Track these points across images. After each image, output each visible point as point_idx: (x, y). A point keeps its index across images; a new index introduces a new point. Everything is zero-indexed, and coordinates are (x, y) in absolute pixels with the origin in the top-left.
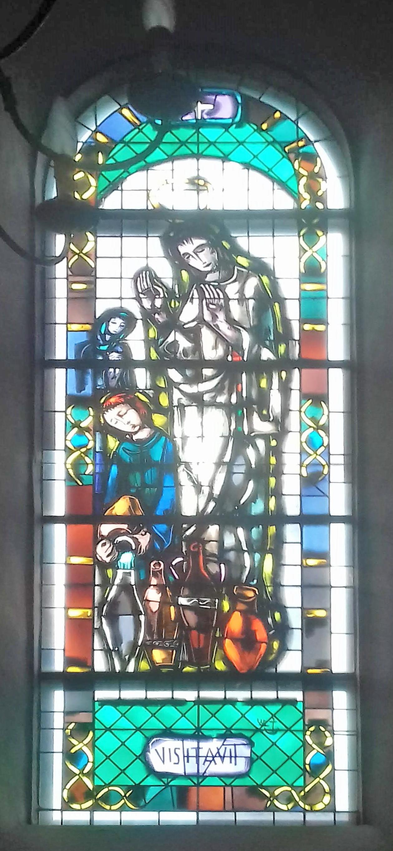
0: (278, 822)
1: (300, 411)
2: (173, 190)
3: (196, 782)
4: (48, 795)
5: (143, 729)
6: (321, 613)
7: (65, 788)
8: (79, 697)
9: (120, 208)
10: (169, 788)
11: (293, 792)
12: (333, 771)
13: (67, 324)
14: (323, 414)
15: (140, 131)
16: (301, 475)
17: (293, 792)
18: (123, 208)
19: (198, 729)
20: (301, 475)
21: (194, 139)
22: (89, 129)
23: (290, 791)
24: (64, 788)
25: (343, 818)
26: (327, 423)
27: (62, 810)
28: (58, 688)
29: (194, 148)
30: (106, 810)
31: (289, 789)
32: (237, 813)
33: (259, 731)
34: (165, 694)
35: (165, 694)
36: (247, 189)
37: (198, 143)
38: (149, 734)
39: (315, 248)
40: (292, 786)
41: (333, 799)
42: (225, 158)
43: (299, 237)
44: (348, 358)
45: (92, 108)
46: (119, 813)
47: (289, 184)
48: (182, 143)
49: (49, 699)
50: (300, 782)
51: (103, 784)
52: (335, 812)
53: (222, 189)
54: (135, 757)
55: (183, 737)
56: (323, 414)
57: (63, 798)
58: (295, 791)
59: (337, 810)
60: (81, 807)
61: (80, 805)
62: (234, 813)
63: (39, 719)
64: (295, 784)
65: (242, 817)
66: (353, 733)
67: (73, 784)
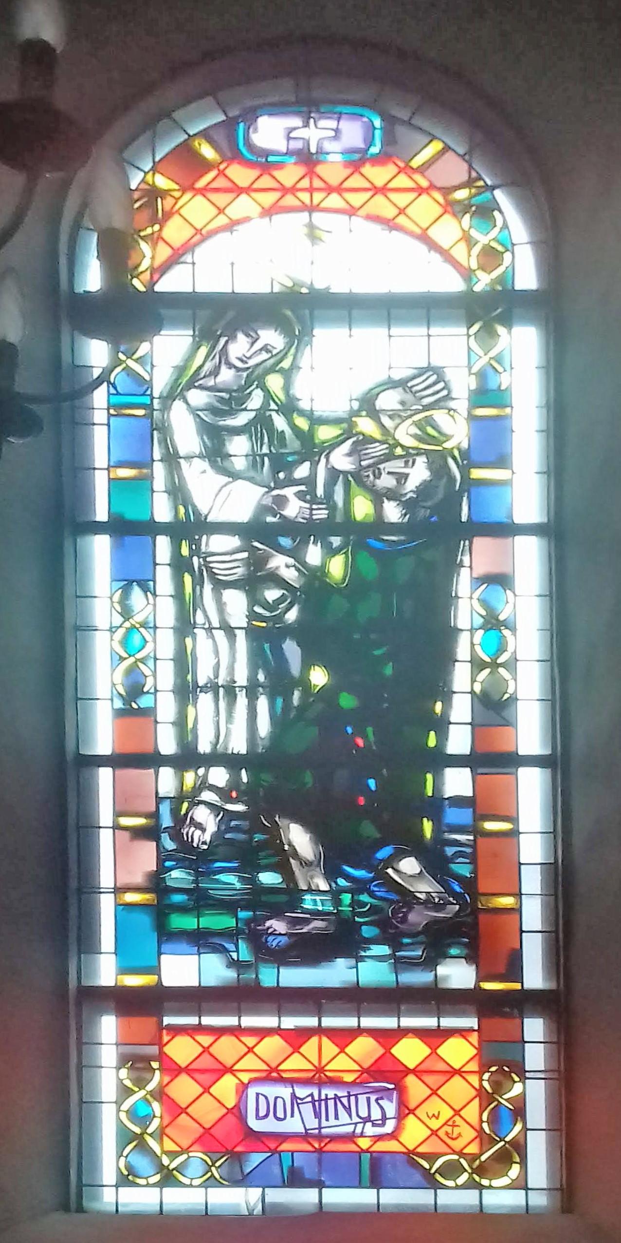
0: (386, 1206)
1: (471, 598)
2: (232, 264)
3: (317, 1146)
4: (95, 1166)
5: (419, 1072)
6: (508, 901)
7: (122, 1155)
8: (144, 1025)
9: (191, 290)
10: (277, 1155)
11: (462, 1161)
12: (523, 1132)
13: (108, 469)
14: (507, 602)
15: (222, 173)
16: (472, 692)
17: (462, 1161)
18: (196, 291)
19: (320, 1070)
20: (472, 692)
21: (305, 183)
22: (138, 168)
23: (458, 1160)
24: (119, 1154)
25: (539, 1200)
26: (512, 617)
27: (117, 1186)
28: (107, 1012)
29: (305, 197)
30: (185, 1186)
31: (456, 1157)
32: (438, 1191)
33: (457, 1073)
34: (230, 1021)
35: (230, 1021)
36: (234, 266)
37: (311, 190)
38: (245, 1077)
39: (492, 354)
40: (461, 1154)
41: (523, 1172)
42: (351, 211)
43: (469, 336)
44: (545, 520)
45: (148, 134)
46: (204, 1189)
47: (453, 252)
48: (285, 191)
49: (94, 1024)
50: (473, 1149)
51: (179, 1149)
52: (526, 1189)
53: (310, 263)
54: (189, 1110)
55: (292, 1082)
56: (507, 602)
57: (118, 1168)
58: (466, 1160)
59: (530, 1186)
60: (456, 1184)
61: (491, 1180)
62: (433, 1191)
63: (80, 1053)
64: (465, 1151)
65: (391, 1197)
66: (555, 1075)
67: (497, 1151)
